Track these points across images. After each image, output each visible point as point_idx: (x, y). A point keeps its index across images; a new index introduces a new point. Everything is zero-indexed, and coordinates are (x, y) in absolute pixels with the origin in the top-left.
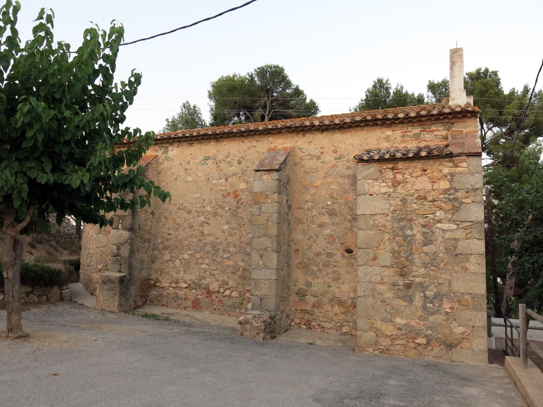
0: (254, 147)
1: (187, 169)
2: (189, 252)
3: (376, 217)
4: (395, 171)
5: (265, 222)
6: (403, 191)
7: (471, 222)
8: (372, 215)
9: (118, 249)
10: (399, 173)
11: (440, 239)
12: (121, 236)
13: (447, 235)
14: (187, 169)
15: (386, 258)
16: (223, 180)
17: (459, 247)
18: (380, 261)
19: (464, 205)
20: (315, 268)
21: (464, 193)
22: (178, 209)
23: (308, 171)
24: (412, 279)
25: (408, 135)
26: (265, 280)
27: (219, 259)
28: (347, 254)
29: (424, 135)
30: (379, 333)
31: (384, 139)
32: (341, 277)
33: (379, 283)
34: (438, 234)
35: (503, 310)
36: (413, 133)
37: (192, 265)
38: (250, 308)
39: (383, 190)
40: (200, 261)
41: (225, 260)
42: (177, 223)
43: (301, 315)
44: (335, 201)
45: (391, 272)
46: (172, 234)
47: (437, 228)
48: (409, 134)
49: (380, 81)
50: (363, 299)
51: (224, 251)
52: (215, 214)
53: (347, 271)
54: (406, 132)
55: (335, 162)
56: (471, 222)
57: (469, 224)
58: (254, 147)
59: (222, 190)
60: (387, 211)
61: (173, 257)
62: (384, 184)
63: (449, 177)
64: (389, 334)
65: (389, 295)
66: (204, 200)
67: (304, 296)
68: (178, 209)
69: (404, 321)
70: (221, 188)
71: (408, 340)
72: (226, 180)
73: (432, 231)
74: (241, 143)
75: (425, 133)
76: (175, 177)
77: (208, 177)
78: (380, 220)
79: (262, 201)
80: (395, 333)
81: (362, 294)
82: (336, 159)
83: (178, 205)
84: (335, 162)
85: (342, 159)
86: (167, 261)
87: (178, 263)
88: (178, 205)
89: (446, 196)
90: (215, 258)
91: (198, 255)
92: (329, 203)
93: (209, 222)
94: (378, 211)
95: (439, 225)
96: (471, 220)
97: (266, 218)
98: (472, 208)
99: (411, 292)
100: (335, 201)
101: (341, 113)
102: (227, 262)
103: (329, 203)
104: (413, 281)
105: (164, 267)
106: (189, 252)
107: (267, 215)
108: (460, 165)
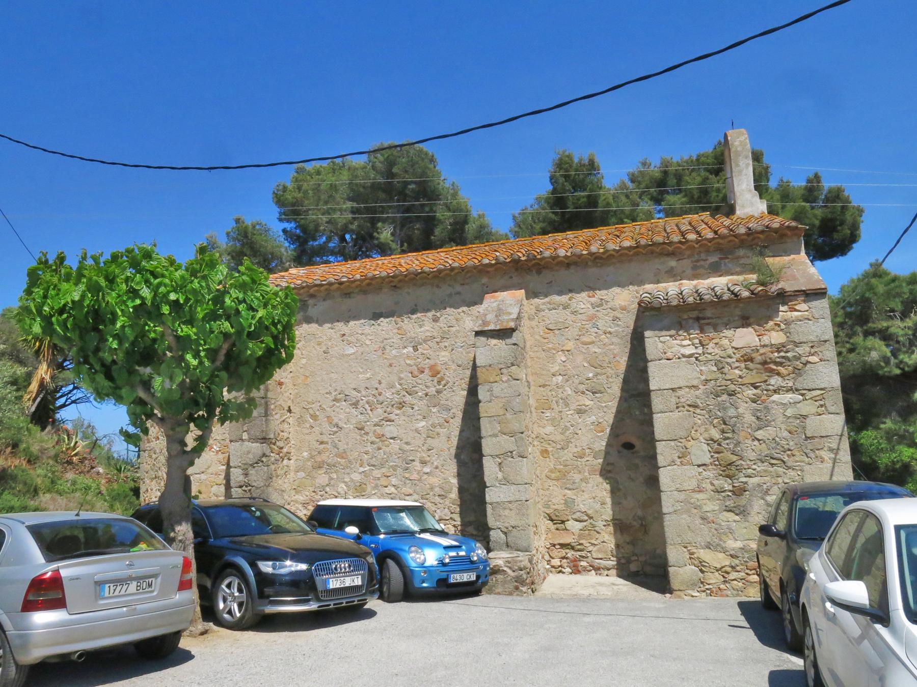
2: (362, 469)
3: (680, 393)
4: (703, 322)
5: (501, 412)
6: (717, 351)
7: (821, 389)
8: (673, 390)
10: (708, 324)
11: (781, 418)
12: (249, 452)
13: (789, 412)
15: (701, 452)
16: (411, 349)
17: (808, 428)
18: (693, 457)
19: (808, 366)
20: (577, 477)
21: (808, 349)
22: (335, 400)
23: (551, 327)
24: (744, 480)
25: (702, 267)
26: (510, 502)
27: (415, 476)
28: (625, 451)
29: (725, 264)
30: (702, 566)
31: (666, 272)
32: (621, 487)
33: (694, 491)
34: (777, 411)
35: (386, 595)
36: (708, 262)
39: (690, 350)
40: (383, 481)
42: (334, 422)
43: (563, 552)
44: (598, 370)
45: (710, 473)
46: (327, 443)
47: (774, 402)
48: (702, 263)
49: (563, 163)
50: (674, 516)
52: (401, 405)
53: (630, 478)
54: (698, 261)
55: (592, 312)
56: (821, 389)
57: (819, 392)
58: (459, 293)
59: (410, 365)
60: (695, 383)
61: (332, 479)
62: (687, 342)
63: (783, 326)
64: (719, 566)
65: (711, 507)
67: (563, 522)
68: (335, 400)
69: (739, 544)
70: (408, 362)
71: (747, 571)
72: (415, 349)
73: (766, 408)
75: (727, 261)
76: (324, 348)
77: (382, 345)
78: (688, 396)
79: (492, 380)
80: (727, 563)
81: (671, 510)
83: (334, 394)
84: (592, 312)
85: (605, 306)
89: (782, 354)
90: (407, 475)
92: (591, 375)
93: (392, 417)
94: (682, 383)
95: (776, 397)
96: (822, 386)
97: (501, 405)
98: (821, 369)
99: (743, 501)
100: (598, 370)
102: (434, 480)
103: (591, 375)
104: (746, 483)
106: (362, 469)
107: (504, 400)
108: (797, 307)
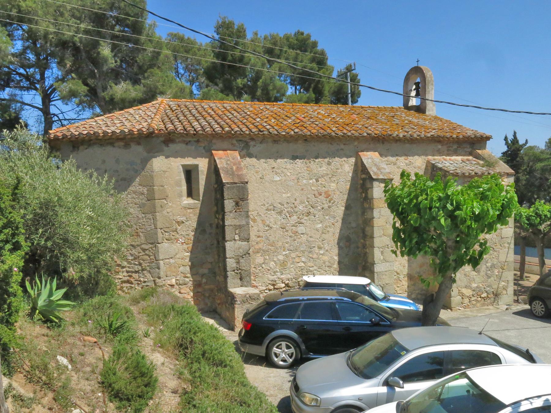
0: (342, 149)
1: (274, 168)
2: (284, 253)
9: (238, 263)
12: (239, 248)
14: (274, 168)
26: (386, 271)
37: (289, 264)
38: (402, 302)
40: (297, 260)
41: (321, 256)
51: (320, 248)
58: (342, 149)
66: (296, 200)
72: (317, 181)
74: (330, 145)
82: (407, 165)
83: (267, 206)
86: (261, 265)
87: (272, 264)
88: (267, 206)
91: (293, 255)
101: (518, 139)
102: (325, 258)
105: (257, 271)
106: (284, 253)
